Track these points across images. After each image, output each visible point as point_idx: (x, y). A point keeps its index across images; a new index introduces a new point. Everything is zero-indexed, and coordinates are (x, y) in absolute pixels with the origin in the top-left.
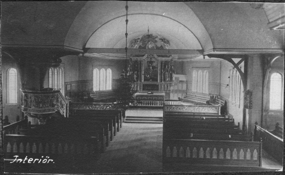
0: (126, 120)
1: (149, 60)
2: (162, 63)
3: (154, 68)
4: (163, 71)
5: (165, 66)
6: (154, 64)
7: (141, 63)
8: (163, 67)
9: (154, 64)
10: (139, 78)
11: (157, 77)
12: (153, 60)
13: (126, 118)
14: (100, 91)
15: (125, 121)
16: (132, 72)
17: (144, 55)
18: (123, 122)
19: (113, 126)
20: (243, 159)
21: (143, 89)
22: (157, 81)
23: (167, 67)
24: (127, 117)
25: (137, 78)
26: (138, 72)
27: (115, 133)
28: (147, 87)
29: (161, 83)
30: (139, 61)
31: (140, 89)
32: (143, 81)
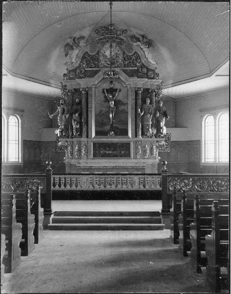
0: (54, 221)
1: (106, 86)
2: (136, 93)
3: (118, 103)
4: (141, 112)
5: (144, 102)
6: (120, 96)
7: (87, 94)
8: (140, 102)
9: (120, 96)
10: (84, 129)
11: (127, 124)
12: (117, 85)
13: (52, 216)
14: (215, 115)
15: (51, 224)
16: (67, 116)
17: (96, 72)
18: (46, 227)
19: (42, 207)
20: (158, 188)
21: (95, 156)
22: (127, 134)
23: (148, 101)
24: (57, 214)
25: (80, 131)
26: (80, 115)
27: (36, 234)
28: (105, 149)
29: (135, 139)
30: (83, 89)
31: (87, 152)
32: (93, 135)
